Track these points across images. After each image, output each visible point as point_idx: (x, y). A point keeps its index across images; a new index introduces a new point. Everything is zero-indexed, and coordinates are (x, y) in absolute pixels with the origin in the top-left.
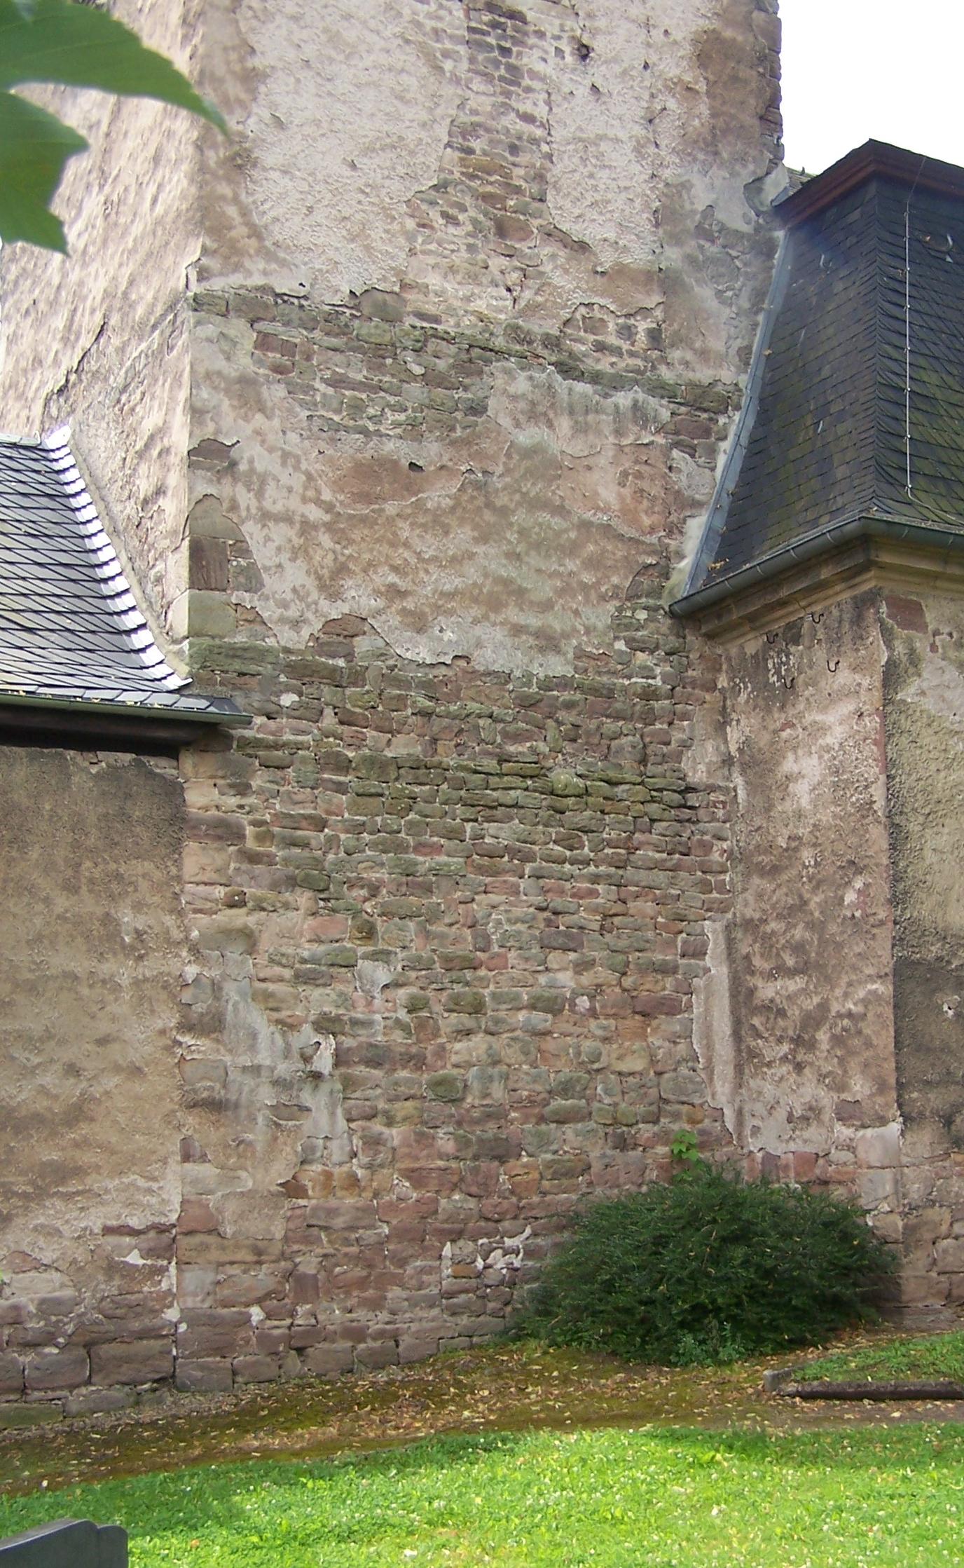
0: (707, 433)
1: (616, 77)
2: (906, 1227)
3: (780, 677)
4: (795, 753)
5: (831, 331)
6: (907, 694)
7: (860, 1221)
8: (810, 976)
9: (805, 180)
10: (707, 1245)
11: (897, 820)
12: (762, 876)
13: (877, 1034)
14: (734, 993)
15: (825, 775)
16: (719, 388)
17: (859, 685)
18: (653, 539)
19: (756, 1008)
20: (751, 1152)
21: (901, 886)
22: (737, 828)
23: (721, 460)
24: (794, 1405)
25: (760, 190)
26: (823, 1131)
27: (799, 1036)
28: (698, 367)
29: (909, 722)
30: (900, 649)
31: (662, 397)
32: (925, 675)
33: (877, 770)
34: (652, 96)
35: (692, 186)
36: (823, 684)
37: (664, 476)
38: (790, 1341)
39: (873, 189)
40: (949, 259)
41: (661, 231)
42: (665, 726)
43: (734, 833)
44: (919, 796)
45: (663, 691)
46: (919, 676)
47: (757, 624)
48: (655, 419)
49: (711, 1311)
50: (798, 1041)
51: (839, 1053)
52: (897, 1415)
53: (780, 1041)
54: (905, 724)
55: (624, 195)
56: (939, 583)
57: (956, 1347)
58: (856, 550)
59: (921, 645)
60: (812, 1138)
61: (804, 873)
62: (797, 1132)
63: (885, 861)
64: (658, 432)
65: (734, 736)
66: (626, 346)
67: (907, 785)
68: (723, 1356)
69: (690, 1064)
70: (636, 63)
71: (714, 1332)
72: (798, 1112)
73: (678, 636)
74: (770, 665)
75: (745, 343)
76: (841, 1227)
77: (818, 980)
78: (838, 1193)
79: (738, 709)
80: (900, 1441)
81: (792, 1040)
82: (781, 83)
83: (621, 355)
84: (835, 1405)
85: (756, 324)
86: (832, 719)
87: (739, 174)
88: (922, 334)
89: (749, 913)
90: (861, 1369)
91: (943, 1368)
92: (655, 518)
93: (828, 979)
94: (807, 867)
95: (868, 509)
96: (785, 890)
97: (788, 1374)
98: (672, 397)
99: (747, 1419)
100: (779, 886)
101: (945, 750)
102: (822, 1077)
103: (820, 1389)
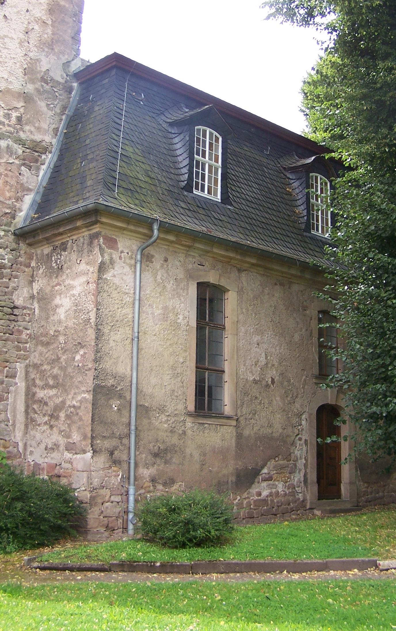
0: (37, 161)
1: (15, 13)
2: (91, 497)
3: (57, 264)
4: (60, 296)
5: (91, 126)
6: (108, 276)
7: (72, 494)
8: (59, 389)
9: (89, 64)
10: (5, 501)
11: (99, 327)
12: (42, 346)
13: (85, 415)
14: (27, 395)
15: (72, 306)
16: (44, 143)
17: (89, 270)
18: (10, 202)
19: (35, 401)
20: (29, 462)
21: (99, 355)
22: (34, 325)
23: (42, 173)
24: (36, 572)
25: (69, 66)
26: (60, 454)
27: (52, 414)
28: (36, 134)
29: (108, 287)
30: (107, 257)
31: (20, 145)
32: (116, 268)
33: (93, 306)
34: (29, 23)
35: (41, 61)
36: (74, 269)
37: (17, 177)
38: (38, 544)
39: (114, 72)
40: (142, 103)
41: (26, 77)
42: (7, 280)
43: (32, 327)
44: (109, 318)
45: (8, 266)
46: (114, 269)
47: (49, 241)
48: (16, 153)
49: (4, 530)
50: (52, 416)
51: (68, 422)
52: (79, 578)
53: (44, 415)
54: (106, 288)
55: (13, 61)
56: (125, 232)
57: (107, 549)
58: (92, 215)
59: (115, 256)
60: (55, 458)
61: (60, 346)
62: (49, 454)
63: (93, 344)
64: (16, 158)
65: (36, 286)
66: (7, 122)
67: (105, 313)
68: (8, 549)
69: (6, 423)
70: (23, 9)
71: (5, 539)
72: (50, 446)
73: (16, 243)
74: (53, 259)
75: (56, 126)
76: (64, 496)
77: (62, 391)
78: (64, 481)
79: (39, 276)
80: (78, 590)
81: (49, 415)
82: (82, 25)
83: (4, 125)
84: (54, 573)
85: (61, 120)
86: (76, 284)
87: (61, 59)
88: (128, 131)
89: (36, 361)
90: (66, 557)
91: (101, 558)
92: (12, 194)
93: (66, 391)
94: (61, 344)
95: (98, 199)
96: (51, 352)
97: (35, 559)
98: (24, 145)
99: (15, 578)
100: (49, 351)
101: (121, 300)
102: (61, 432)
103: (48, 565)
